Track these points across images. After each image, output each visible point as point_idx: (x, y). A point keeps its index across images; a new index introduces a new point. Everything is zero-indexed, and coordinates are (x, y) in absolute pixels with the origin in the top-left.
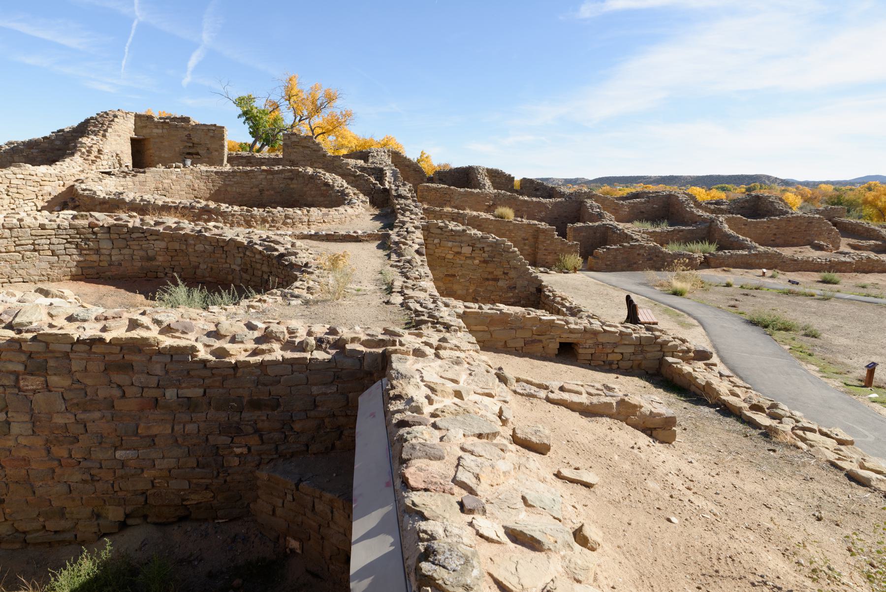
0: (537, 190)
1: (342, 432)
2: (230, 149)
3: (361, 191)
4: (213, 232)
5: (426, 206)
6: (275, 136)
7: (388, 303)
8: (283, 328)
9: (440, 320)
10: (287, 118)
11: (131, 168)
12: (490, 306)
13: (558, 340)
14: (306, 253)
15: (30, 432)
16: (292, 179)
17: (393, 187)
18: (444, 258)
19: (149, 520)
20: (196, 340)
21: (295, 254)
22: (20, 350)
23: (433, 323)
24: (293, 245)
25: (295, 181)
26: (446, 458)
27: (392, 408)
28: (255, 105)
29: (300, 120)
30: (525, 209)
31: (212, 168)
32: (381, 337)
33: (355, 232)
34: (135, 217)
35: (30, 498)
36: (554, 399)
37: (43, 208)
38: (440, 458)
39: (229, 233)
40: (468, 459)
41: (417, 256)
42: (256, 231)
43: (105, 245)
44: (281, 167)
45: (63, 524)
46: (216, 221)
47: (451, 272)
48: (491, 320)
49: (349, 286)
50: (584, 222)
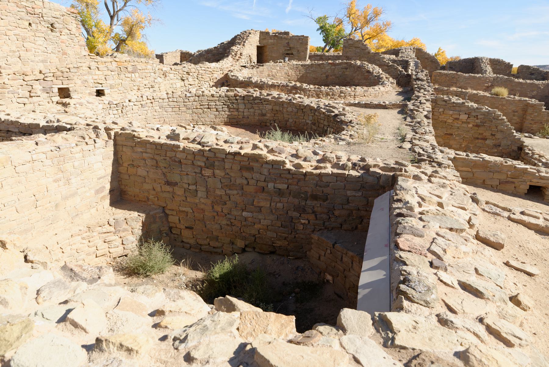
0: (532, 74)
1: (362, 220)
2: (310, 51)
3: (391, 76)
4: (298, 100)
5: (437, 87)
6: (338, 41)
7: (400, 147)
8: (333, 155)
9: (435, 160)
10: (347, 29)
11: (256, 63)
12: (475, 155)
13: (529, 183)
14: (351, 114)
15: (206, 197)
16: (346, 69)
17: (414, 73)
18: (446, 122)
19: (256, 250)
20: (286, 158)
21: (344, 115)
22: (203, 155)
23: (430, 161)
24: (344, 109)
25: (348, 70)
26: (425, 237)
27: (394, 206)
28: (328, 22)
29: (355, 30)
30: (519, 89)
31: (300, 63)
32: (392, 166)
33: (384, 103)
34: (257, 91)
35: (204, 229)
36: (514, 219)
37: (213, 86)
38: (421, 236)
39: (307, 101)
40: (440, 240)
41: (425, 119)
42: (322, 100)
43: (242, 106)
44: (340, 61)
45: (217, 244)
46: (300, 94)
47: (449, 132)
48: (475, 164)
49: (376, 136)
50: (526, 83)
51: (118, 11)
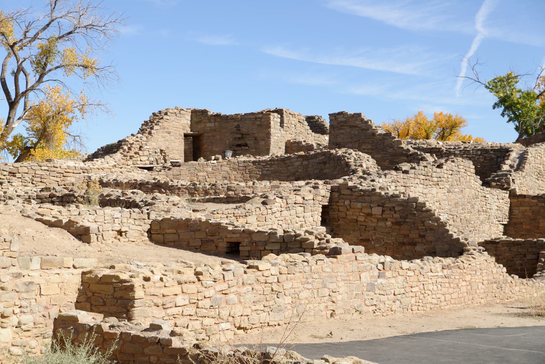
16: (325, 163)
25: (327, 165)
28: (518, 86)
51: (24, 93)
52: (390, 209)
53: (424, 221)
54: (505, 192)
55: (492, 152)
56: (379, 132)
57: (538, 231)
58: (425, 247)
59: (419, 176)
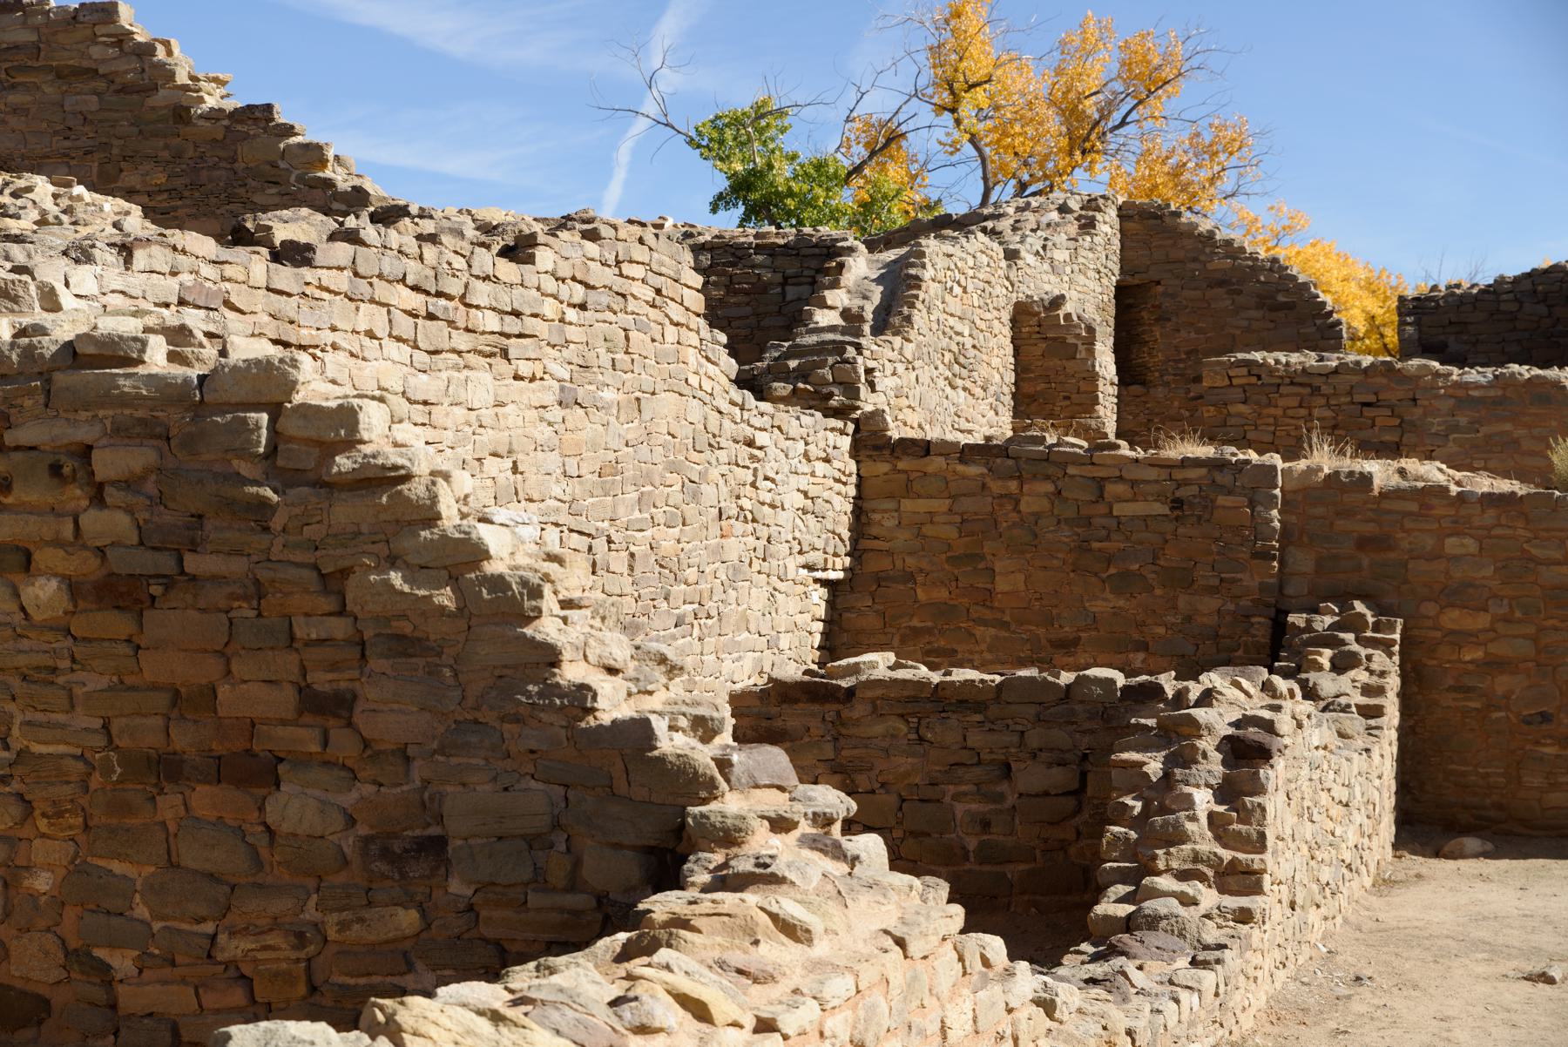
28: (788, 143)
52: (55, 469)
53: (345, 573)
54: (839, 424)
55: (760, 258)
56: (211, 102)
57: (988, 614)
58: (349, 799)
59: (382, 291)
